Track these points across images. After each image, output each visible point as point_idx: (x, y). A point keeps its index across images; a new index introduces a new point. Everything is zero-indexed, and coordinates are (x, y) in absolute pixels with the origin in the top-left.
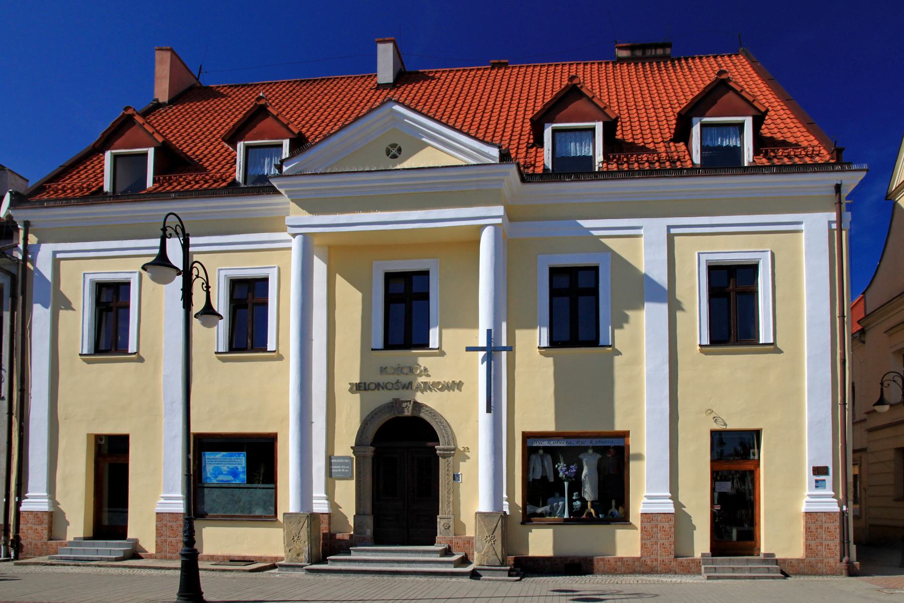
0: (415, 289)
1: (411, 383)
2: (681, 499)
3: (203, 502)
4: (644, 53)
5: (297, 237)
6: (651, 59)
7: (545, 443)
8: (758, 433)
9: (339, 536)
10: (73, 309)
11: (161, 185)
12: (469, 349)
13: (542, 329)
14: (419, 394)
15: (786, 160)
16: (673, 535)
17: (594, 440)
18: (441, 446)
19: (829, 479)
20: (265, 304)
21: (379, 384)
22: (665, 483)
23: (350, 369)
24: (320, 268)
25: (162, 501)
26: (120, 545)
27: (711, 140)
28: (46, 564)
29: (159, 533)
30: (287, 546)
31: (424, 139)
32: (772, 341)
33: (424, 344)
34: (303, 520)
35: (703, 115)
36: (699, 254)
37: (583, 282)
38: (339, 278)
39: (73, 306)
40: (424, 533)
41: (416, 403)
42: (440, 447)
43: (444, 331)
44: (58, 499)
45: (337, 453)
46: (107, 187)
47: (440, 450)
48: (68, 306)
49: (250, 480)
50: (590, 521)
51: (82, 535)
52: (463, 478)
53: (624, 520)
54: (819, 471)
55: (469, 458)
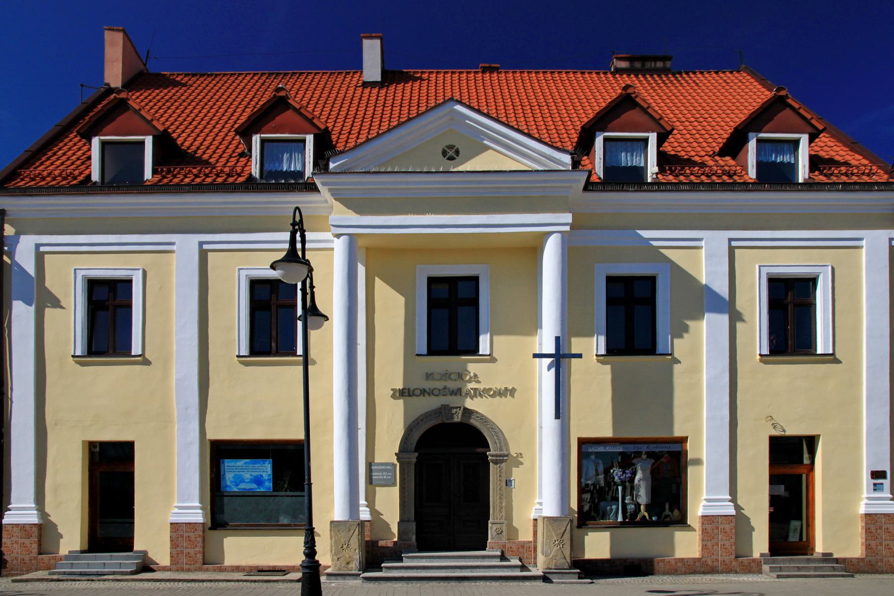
1: (460, 390)
2: (378, 507)
3: (222, 512)
4: (643, 65)
5: (342, 238)
6: (652, 72)
7: (601, 449)
8: (811, 442)
9: (381, 543)
10: (63, 308)
11: (164, 177)
12: (536, 356)
14: (468, 400)
15: (703, 178)
16: (734, 536)
17: (652, 446)
18: (492, 452)
19: (887, 482)
20: (129, 306)
21: (424, 390)
22: (721, 486)
23: (392, 372)
24: (361, 270)
25: (176, 510)
26: (127, 558)
27: (765, 155)
28: (47, 580)
29: (174, 543)
30: (336, 554)
32: (831, 352)
33: (473, 350)
35: (760, 131)
36: (760, 266)
37: (463, 292)
38: (378, 282)
39: (62, 304)
40: (477, 540)
41: (465, 409)
42: (492, 451)
43: (495, 338)
44: (47, 510)
45: (378, 459)
46: (96, 177)
47: (492, 456)
48: (56, 303)
49: (277, 486)
50: (644, 523)
51: (78, 549)
53: (681, 521)
54: (877, 475)
55: (522, 464)
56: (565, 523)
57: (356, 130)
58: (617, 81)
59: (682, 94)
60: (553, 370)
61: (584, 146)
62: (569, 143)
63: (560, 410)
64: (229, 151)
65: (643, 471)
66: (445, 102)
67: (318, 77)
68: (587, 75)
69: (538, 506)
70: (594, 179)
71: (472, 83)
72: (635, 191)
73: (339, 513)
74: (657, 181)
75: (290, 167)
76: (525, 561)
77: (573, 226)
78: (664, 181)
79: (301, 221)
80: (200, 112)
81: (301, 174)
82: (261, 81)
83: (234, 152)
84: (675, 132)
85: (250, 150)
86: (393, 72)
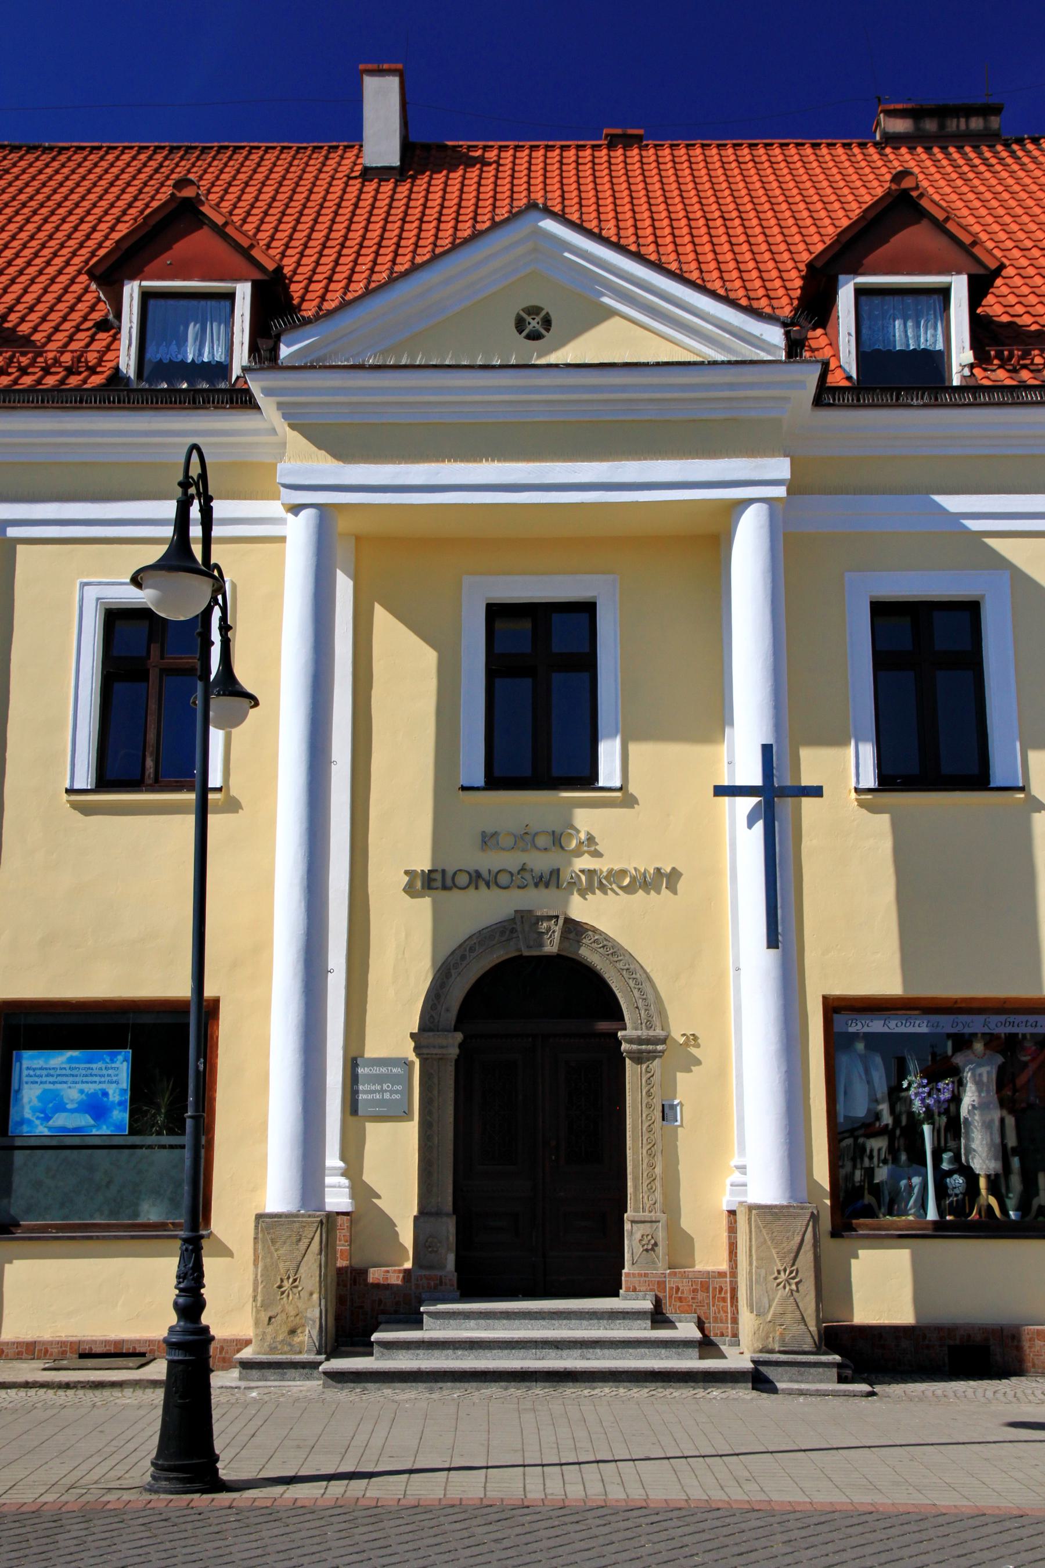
0: (558, 646)
1: (556, 873)
2: (369, 1177)
4: (942, 126)
5: (305, 513)
6: (961, 139)
7: (877, 1026)
9: (375, 1275)
12: (721, 791)
13: (861, 747)
14: (576, 898)
17: (994, 1019)
21: (478, 875)
23: (406, 834)
24: (344, 586)
30: (265, 1306)
31: (606, 300)
33: (585, 777)
34: (308, 1232)
38: (381, 616)
41: (568, 921)
42: (629, 1032)
43: (632, 747)
45: (373, 1050)
47: (630, 1041)
50: (992, 1228)
52: (685, 1115)
55: (698, 1062)
56: (800, 1223)
57: (344, 270)
58: (887, 162)
59: (1024, 188)
60: (759, 826)
61: (815, 306)
62: (785, 300)
63: (780, 928)
64: (76, 316)
65: (979, 1083)
66: (514, 216)
67: (271, 156)
68: (824, 151)
69: (736, 1177)
70: (835, 379)
71: (587, 170)
72: (925, 406)
73: (277, 1194)
74: (972, 382)
75: (201, 354)
76: (711, 1327)
77: (795, 487)
78: (986, 382)
79: (203, 476)
80: (21, 229)
81: (223, 369)
82: (153, 164)
83: (85, 319)
84: (1010, 271)
85: (118, 315)
86: (427, 147)
